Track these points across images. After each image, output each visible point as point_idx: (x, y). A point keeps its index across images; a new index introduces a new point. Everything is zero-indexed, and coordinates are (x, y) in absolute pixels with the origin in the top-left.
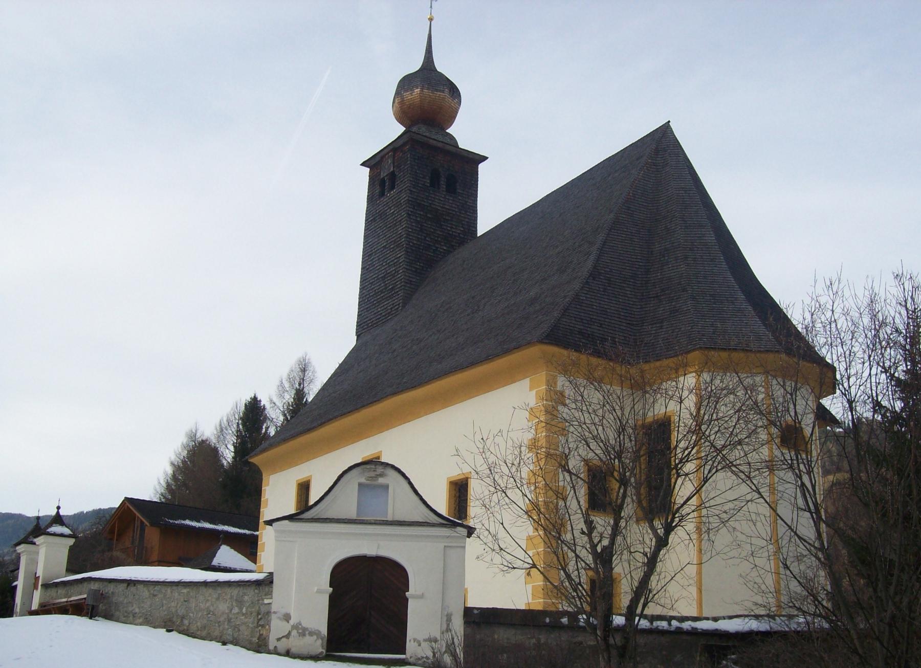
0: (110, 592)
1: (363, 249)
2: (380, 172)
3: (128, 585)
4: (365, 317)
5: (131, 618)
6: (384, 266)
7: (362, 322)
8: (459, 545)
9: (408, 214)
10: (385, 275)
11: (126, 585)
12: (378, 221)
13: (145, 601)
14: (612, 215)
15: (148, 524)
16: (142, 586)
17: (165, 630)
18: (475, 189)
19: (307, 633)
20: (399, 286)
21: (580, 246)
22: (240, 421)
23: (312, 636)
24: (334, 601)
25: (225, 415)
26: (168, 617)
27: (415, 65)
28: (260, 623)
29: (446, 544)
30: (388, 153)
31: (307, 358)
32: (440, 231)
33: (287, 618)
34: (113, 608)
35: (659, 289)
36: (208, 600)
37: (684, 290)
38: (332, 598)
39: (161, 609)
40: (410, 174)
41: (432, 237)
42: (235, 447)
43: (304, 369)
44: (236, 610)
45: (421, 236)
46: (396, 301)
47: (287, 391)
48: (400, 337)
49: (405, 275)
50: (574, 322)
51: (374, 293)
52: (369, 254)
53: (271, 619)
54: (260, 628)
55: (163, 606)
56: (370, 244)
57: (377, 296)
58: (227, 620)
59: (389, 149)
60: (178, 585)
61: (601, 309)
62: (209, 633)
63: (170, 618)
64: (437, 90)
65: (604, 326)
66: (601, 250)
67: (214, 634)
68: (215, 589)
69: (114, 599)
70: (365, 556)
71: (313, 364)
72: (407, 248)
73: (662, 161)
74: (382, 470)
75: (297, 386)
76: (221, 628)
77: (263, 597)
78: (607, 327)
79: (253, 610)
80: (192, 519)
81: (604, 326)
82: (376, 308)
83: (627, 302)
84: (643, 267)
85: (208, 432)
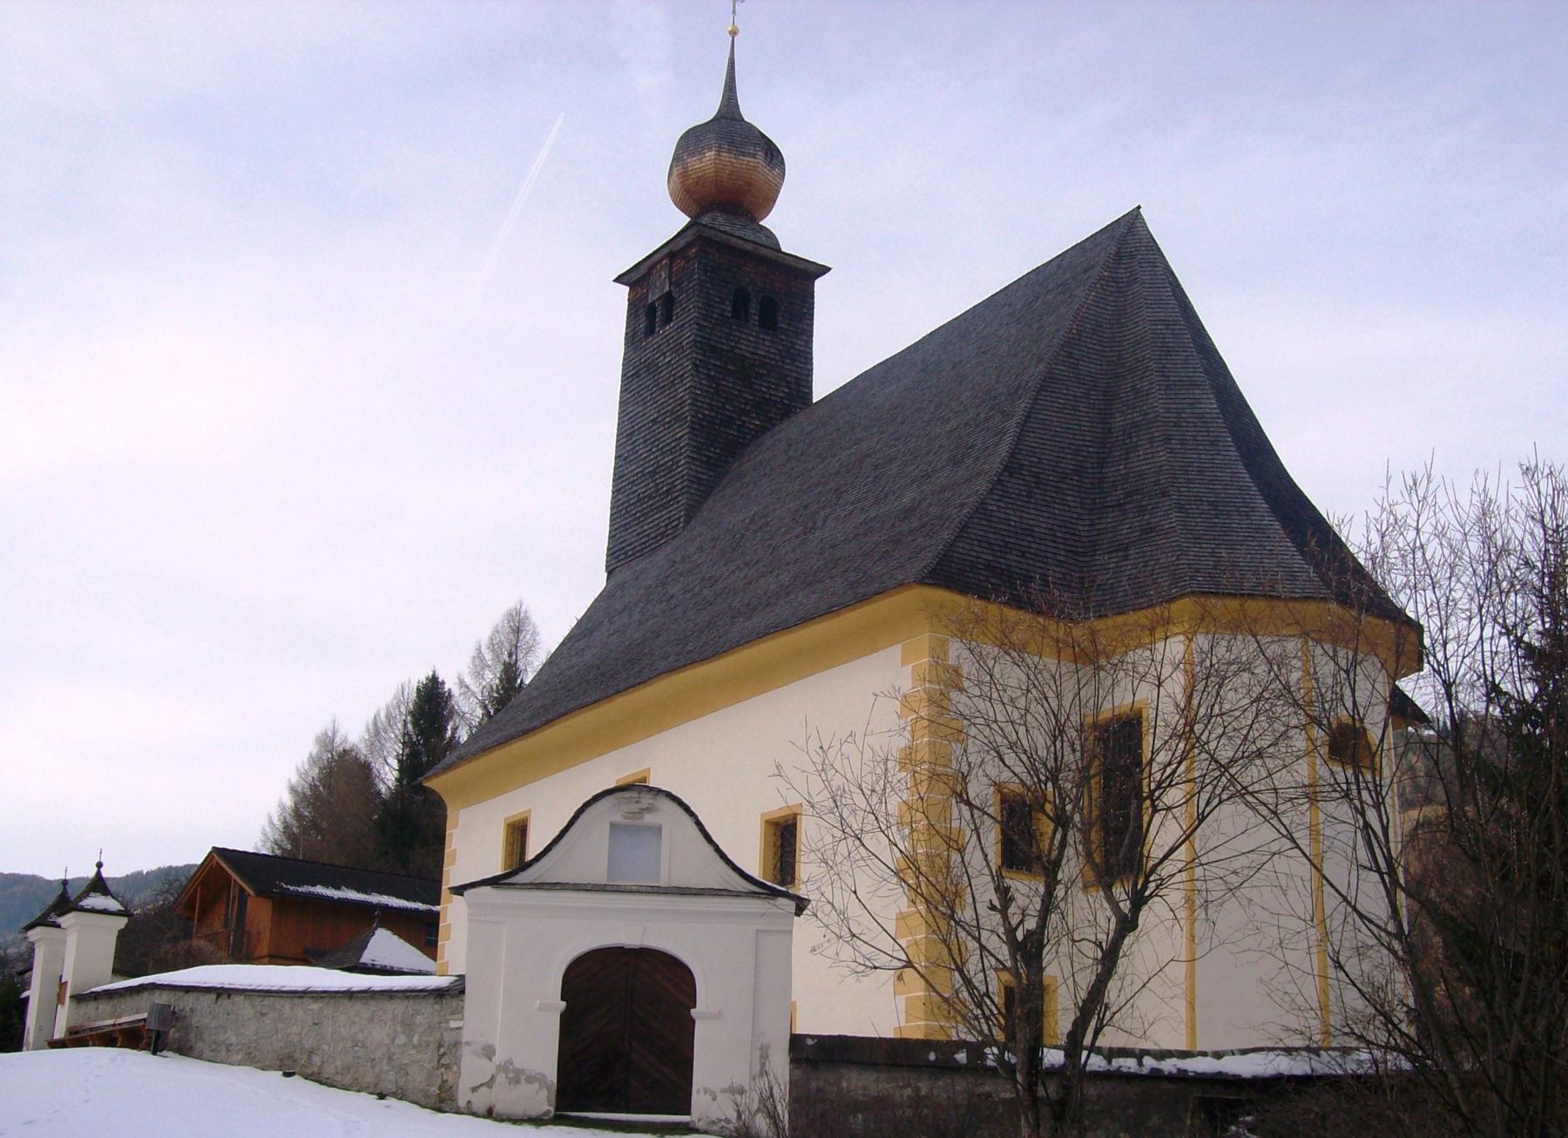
0: (187, 1009)
3: (218, 996)
4: (621, 540)
7: (615, 549)
9: (694, 364)
11: (215, 997)
14: (1042, 367)
15: (252, 893)
16: (242, 997)
17: (281, 1073)
19: (523, 1077)
20: (679, 487)
21: (987, 419)
22: (409, 718)
23: (531, 1083)
24: (569, 1023)
26: (286, 1051)
27: (707, 109)
28: (443, 1061)
29: (760, 928)
30: (660, 261)
31: (523, 609)
33: (489, 1052)
34: (192, 1036)
37: (1164, 494)
38: (566, 1019)
44: (402, 1039)
45: (717, 401)
47: (489, 666)
48: (680, 574)
50: (977, 548)
54: (443, 1070)
57: (641, 505)
61: (1024, 526)
64: (744, 154)
69: (194, 1021)
72: (693, 422)
74: (651, 801)
76: (376, 1070)
78: (1033, 557)
80: (326, 885)
84: (1095, 455)
85: (354, 734)
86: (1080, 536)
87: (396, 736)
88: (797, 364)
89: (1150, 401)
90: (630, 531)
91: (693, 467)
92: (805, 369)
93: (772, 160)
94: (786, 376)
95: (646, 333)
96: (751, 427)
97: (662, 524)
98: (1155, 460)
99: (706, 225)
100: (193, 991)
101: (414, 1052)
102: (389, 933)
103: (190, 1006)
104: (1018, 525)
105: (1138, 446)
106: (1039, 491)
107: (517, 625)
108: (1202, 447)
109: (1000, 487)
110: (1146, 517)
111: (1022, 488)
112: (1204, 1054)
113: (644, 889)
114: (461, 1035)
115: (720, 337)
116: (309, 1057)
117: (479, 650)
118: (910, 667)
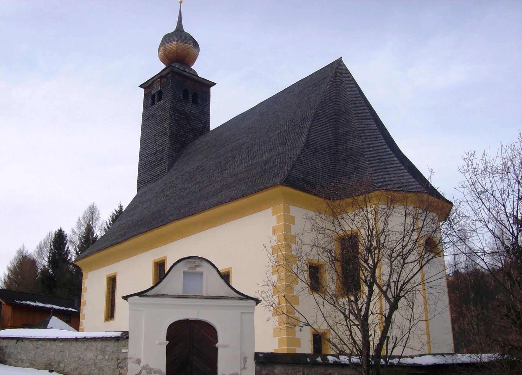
0: (4, 346)
1: (141, 137)
2: (152, 90)
3: (17, 341)
4: (143, 177)
5: (20, 363)
6: (155, 146)
7: (140, 180)
8: (250, 311)
9: (171, 115)
10: (156, 152)
11: (16, 341)
12: (150, 119)
13: (31, 351)
14: (313, 111)
15: (5, 304)
16: (28, 341)
17: (48, 371)
18: (209, 102)
19: (152, 371)
20: (165, 158)
21: (293, 129)
22: (52, 244)
24: (169, 349)
25: (43, 240)
26: (48, 362)
27: (172, 28)
28: (120, 365)
29: (242, 311)
30: (157, 79)
31: (95, 205)
32: (190, 126)
33: (139, 362)
34: (6, 356)
35: (345, 155)
36: (79, 351)
37: (362, 156)
38: (168, 347)
39: (43, 357)
40: (172, 91)
41: (185, 129)
42: (49, 259)
43: (93, 212)
44: (100, 357)
45: (178, 128)
46: (163, 167)
47: (83, 225)
48: (170, 188)
49: (169, 151)
50: (298, 173)
51: (148, 163)
52: (145, 139)
53: (128, 363)
54: (120, 369)
55: (44, 355)
56: (146, 133)
57: (151, 164)
58: (93, 364)
59: (157, 77)
60: (55, 341)
61: (313, 166)
62: (80, 373)
63: (49, 363)
64: (186, 43)
65: (315, 177)
66: (309, 131)
67: (84, 373)
68: (83, 343)
69: (7, 350)
70: (188, 320)
71: (98, 210)
72: (170, 135)
73: (340, 80)
74: (199, 263)
75: (88, 222)
76: (89, 369)
77: (121, 348)
78: (317, 177)
79: (114, 356)
80: (31, 301)
81: (315, 177)
82: (150, 172)
83: (326, 162)
84: (334, 142)
85: (31, 250)
86: (331, 170)
87: (47, 250)
88: (205, 116)
89: (352, 124)
90: (146, 174)
91: (170, 151)
92: (207, 118)
93: (195, 46)
94: (201, 120)
95: (151, 105)
96: (190, 137)
97: (159, 171)
98: (356, 144)
99: (173, 66)
100: (6, 339)
101: (106, 362)
102: (56, 318)
103: (5, 345)
104: (311, 166)
105: (349, 139)
106: (317, 154)
107: (92, 211)
108: (372, 140)
109: (304, 152)
110: (356, 164)
111: (311, 153)
112: (407, 357)
113: (198, 297)
114: (127, 355)
115: (179, 106)
116: (59, 365)
117: (79, 219)
118: (276, 216)
